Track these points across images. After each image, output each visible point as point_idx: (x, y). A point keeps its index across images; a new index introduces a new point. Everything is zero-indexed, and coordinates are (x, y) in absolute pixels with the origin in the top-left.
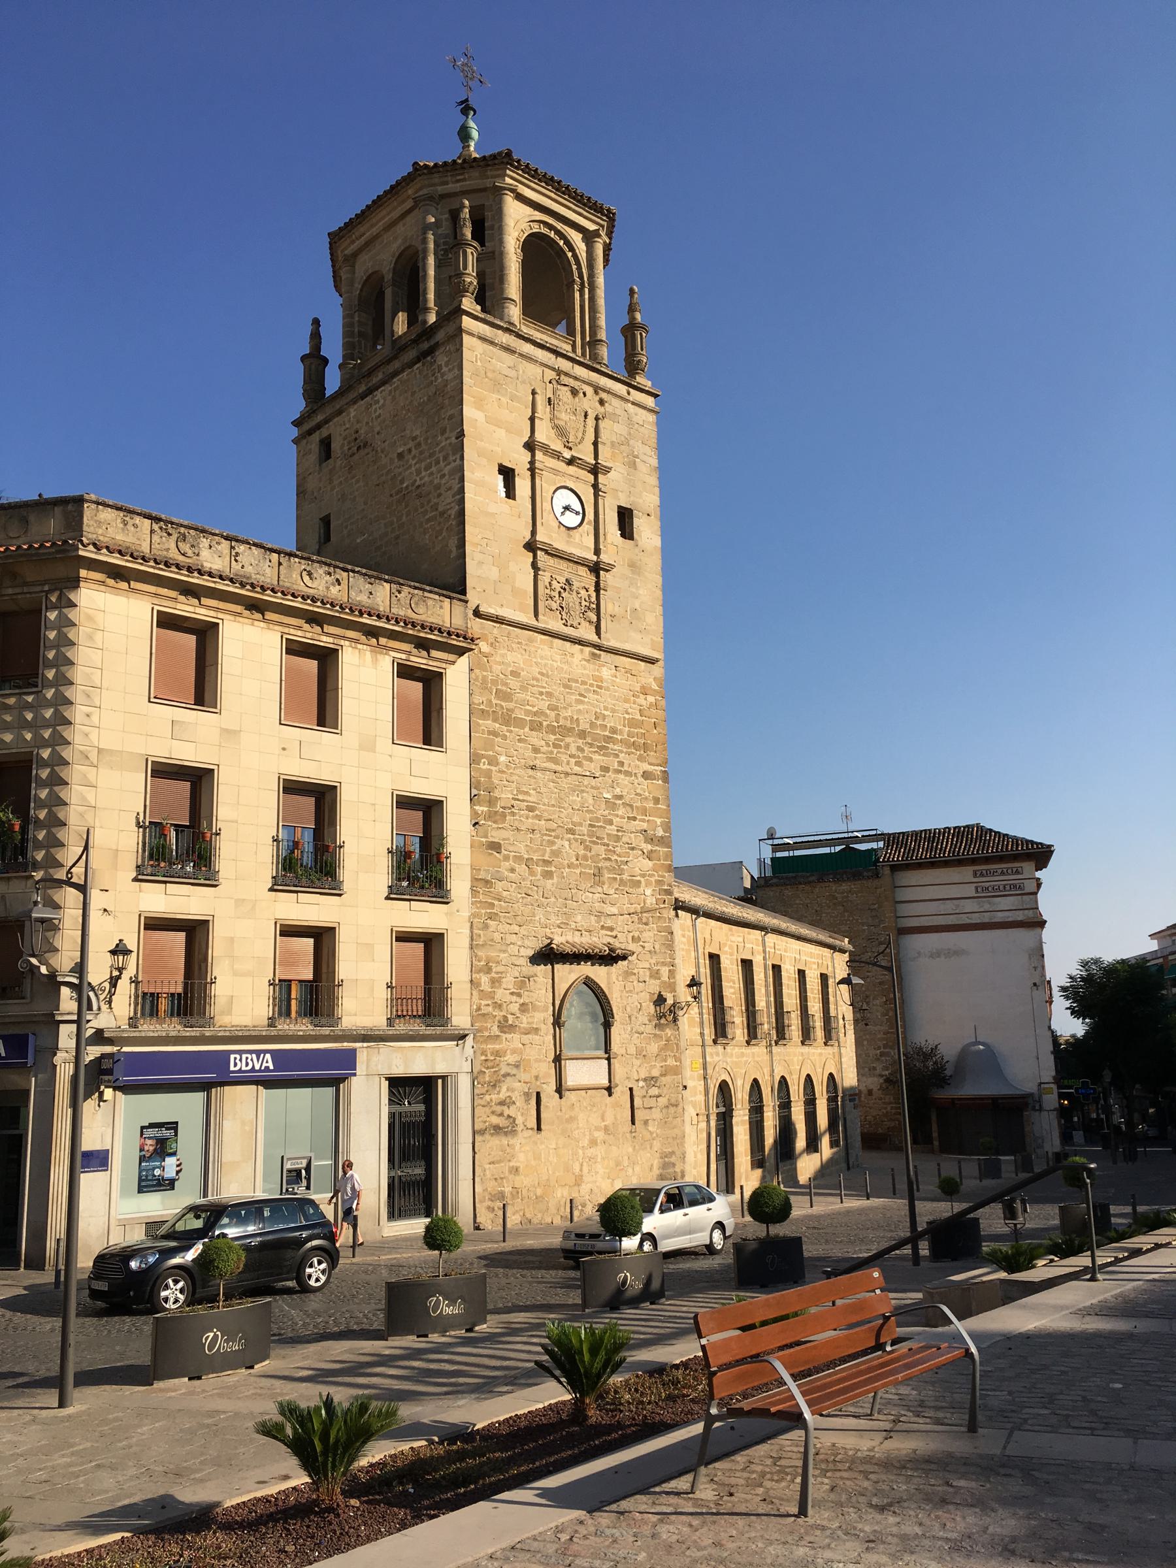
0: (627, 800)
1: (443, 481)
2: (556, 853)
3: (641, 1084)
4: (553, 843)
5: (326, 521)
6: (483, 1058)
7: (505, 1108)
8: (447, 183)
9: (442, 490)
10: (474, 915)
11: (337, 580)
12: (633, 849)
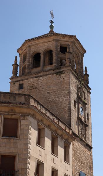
1: (63, 101)
8: (61, 38)
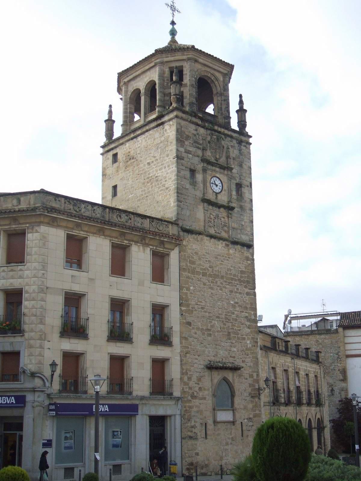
0: (240, 303)
1: (167, 175)
2: (212, 326)
3: (246, 420)
4: (211, 322)
5: (115, 187)
6: (185, 409)
7: (193, 429)
9: (167, 179)
10: (181, 352)
11: (130, 218)
12: (242, 324)
